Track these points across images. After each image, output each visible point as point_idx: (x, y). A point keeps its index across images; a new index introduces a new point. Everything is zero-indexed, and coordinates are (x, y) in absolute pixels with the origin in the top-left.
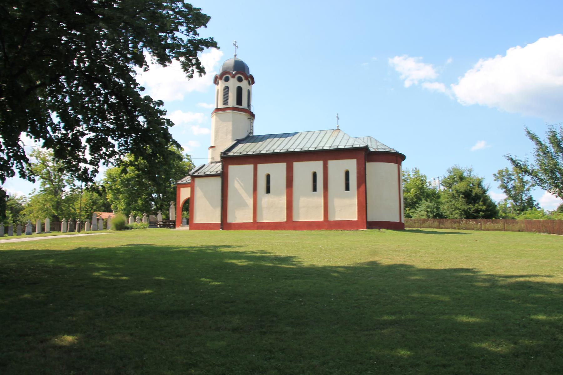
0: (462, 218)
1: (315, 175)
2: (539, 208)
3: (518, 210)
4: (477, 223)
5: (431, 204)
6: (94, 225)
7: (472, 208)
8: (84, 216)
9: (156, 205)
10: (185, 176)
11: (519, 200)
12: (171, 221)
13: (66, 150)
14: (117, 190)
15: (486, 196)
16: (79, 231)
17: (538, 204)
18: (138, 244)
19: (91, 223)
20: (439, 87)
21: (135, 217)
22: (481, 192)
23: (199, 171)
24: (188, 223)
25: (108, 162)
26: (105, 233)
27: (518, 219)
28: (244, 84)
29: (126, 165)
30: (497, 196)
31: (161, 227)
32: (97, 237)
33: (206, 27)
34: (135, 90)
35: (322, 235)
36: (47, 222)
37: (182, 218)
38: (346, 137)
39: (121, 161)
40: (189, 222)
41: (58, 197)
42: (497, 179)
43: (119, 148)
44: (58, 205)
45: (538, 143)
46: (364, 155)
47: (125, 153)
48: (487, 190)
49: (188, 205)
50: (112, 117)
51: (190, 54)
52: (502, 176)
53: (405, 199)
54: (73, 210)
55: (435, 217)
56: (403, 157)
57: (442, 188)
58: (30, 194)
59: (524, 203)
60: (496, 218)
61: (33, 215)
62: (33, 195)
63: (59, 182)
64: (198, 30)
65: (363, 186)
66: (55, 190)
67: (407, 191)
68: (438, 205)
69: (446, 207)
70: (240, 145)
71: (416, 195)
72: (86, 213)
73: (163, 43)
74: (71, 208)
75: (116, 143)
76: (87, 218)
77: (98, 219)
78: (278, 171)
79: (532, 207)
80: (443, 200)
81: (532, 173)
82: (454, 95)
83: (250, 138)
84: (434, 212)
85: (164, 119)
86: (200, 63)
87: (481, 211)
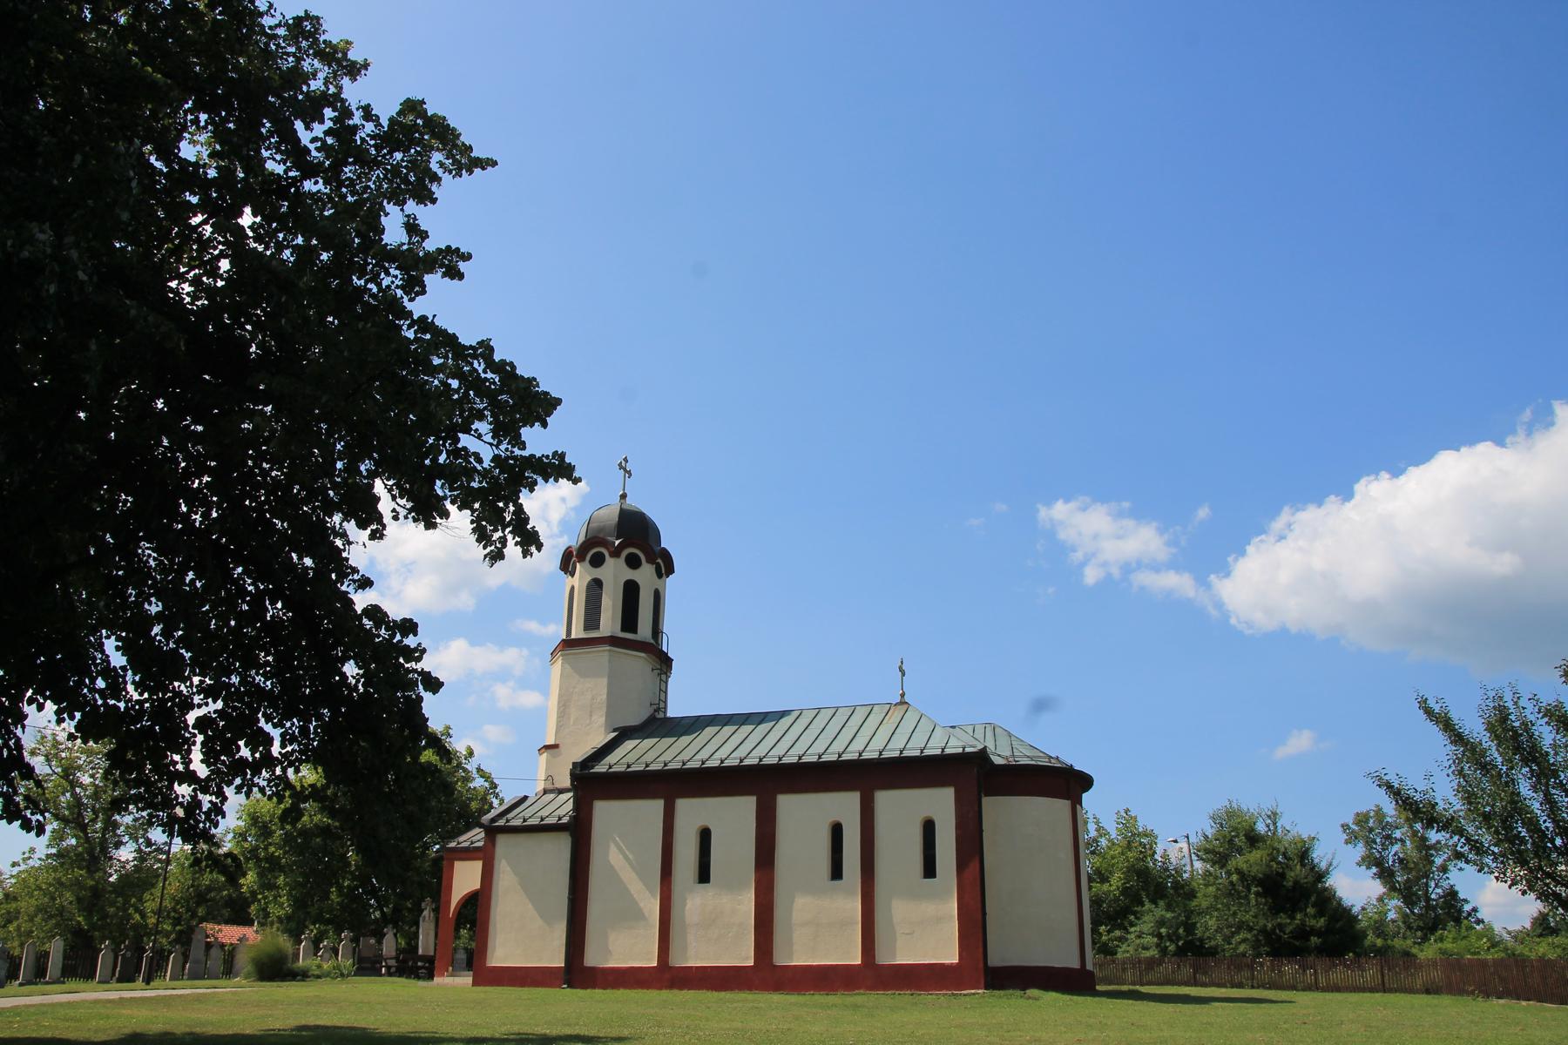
0: (1259, 955)
1: (837, 831)
2: (1479, 921)
3: (1419, 928)
4: (1304, 968)
5: (1169, 915)
6: (196, 962)
7: (1289, 924)
8: (167, 935)
9: (380, 908)
10: (468, 828)
11: (1419, 898)
12: (423, 958)
13: (138, 751)
14: (271, 859)
15: (1326, 889)
16: (148, 981)
17: (1475, 910)
18: (317, 1027)
19: (186, 957)
20: (1178, 582)
21: (316, 943)
22: (1310, 879)
23: (510, 816)
24: (469, 965)
25: (251, 785)
26: (225, 989)
27: (1422, 956)
28: (645, 575)
29: (299, 795)
30: (1356, 887)
31: (389, 974)
32: (199, 999)
33: (545, 425)
34: (344, 588)
35: (856, 1007)
36: (56, 948)
37: (455, 950)
38: (925, 727)
39: (289, 785)
40: (474, 961)
41: (98, 875)
42: (1352, 838)
43: (283, 746)
44: (93, 899)
45: (1457, 737)
46: (975, 776)
47: (301, 762)
48: (1327, 872)
49: (476, 909)
50: (270, 658)
51: (497, 505)
52: (1364, 829)
53: (1096, 902)
54: (137, 917)
55: (1181, 952)
56: (1085, 782)
57: (1198, 865)
58: (14, 864)
59: (1434, 908)
60: (1358, 955)
61: (19, 928)
62: (23, 867)
63: (104, 830)
64: (526, 433)
65: (974, 865)
66: (91, 852)
67: (1101, 876)
68: (1188, 918)
69: (1212, 923)
70: (629, 744)
71: (1125, 891)
72: (174, 925)
73: (427, 462)
74: (131, 910)
75: (276, 733)
76: (176, 941)
77: (209, 946)
78: (732, 818)
79: (1458, 921)
80: (1202, 902)
81: (1448, 824)
82: (1219, 605)
83: (658, 725)
84: (1179, 938)
85: (415, 671)
86: (527, 520)
87: (1313, 932)
